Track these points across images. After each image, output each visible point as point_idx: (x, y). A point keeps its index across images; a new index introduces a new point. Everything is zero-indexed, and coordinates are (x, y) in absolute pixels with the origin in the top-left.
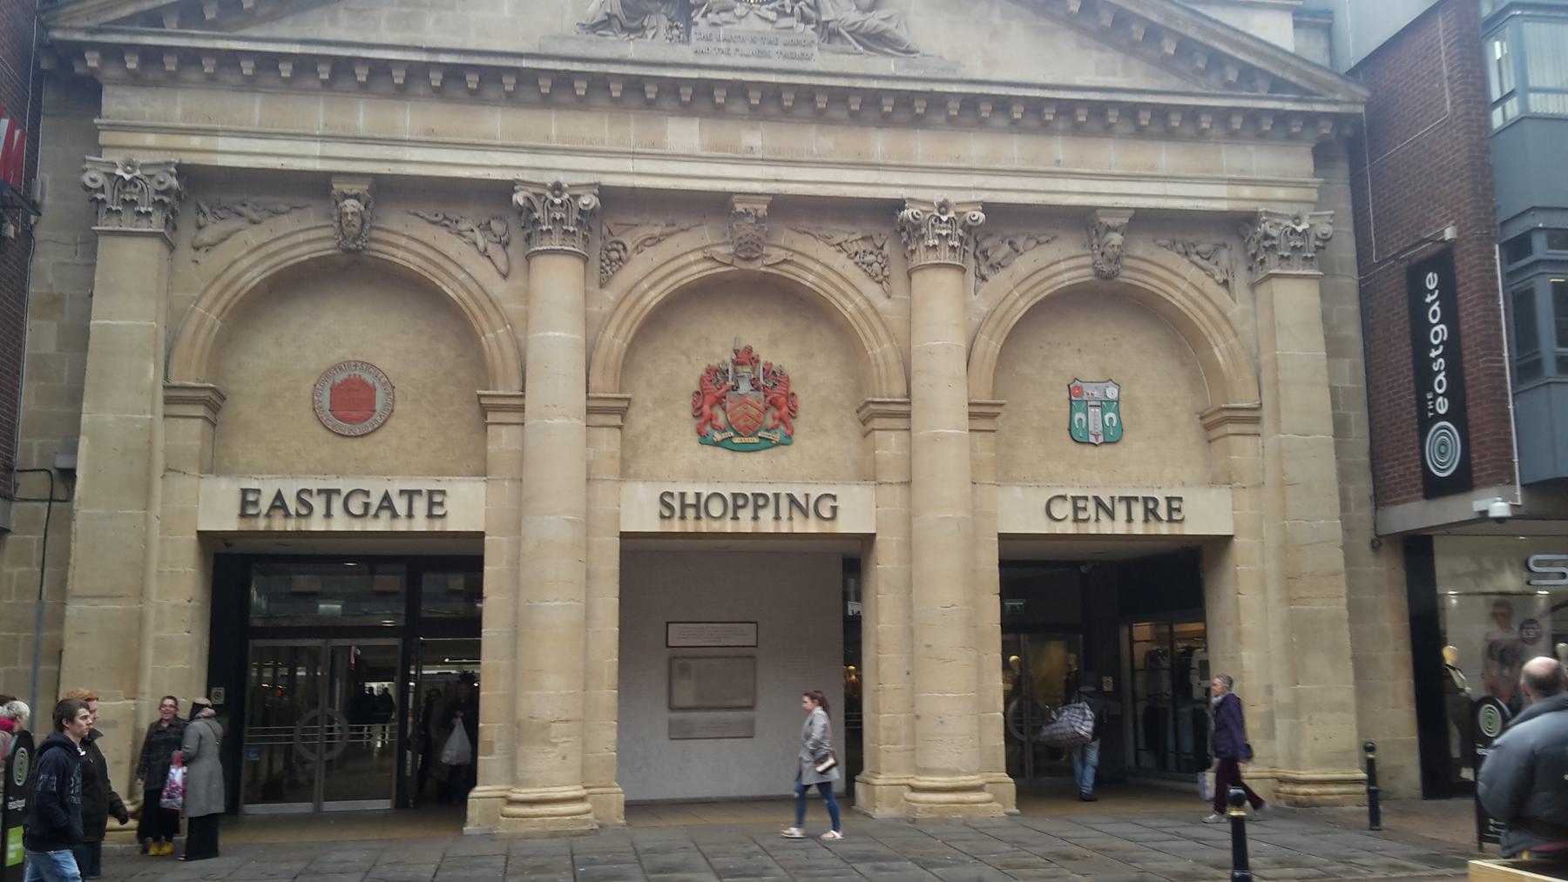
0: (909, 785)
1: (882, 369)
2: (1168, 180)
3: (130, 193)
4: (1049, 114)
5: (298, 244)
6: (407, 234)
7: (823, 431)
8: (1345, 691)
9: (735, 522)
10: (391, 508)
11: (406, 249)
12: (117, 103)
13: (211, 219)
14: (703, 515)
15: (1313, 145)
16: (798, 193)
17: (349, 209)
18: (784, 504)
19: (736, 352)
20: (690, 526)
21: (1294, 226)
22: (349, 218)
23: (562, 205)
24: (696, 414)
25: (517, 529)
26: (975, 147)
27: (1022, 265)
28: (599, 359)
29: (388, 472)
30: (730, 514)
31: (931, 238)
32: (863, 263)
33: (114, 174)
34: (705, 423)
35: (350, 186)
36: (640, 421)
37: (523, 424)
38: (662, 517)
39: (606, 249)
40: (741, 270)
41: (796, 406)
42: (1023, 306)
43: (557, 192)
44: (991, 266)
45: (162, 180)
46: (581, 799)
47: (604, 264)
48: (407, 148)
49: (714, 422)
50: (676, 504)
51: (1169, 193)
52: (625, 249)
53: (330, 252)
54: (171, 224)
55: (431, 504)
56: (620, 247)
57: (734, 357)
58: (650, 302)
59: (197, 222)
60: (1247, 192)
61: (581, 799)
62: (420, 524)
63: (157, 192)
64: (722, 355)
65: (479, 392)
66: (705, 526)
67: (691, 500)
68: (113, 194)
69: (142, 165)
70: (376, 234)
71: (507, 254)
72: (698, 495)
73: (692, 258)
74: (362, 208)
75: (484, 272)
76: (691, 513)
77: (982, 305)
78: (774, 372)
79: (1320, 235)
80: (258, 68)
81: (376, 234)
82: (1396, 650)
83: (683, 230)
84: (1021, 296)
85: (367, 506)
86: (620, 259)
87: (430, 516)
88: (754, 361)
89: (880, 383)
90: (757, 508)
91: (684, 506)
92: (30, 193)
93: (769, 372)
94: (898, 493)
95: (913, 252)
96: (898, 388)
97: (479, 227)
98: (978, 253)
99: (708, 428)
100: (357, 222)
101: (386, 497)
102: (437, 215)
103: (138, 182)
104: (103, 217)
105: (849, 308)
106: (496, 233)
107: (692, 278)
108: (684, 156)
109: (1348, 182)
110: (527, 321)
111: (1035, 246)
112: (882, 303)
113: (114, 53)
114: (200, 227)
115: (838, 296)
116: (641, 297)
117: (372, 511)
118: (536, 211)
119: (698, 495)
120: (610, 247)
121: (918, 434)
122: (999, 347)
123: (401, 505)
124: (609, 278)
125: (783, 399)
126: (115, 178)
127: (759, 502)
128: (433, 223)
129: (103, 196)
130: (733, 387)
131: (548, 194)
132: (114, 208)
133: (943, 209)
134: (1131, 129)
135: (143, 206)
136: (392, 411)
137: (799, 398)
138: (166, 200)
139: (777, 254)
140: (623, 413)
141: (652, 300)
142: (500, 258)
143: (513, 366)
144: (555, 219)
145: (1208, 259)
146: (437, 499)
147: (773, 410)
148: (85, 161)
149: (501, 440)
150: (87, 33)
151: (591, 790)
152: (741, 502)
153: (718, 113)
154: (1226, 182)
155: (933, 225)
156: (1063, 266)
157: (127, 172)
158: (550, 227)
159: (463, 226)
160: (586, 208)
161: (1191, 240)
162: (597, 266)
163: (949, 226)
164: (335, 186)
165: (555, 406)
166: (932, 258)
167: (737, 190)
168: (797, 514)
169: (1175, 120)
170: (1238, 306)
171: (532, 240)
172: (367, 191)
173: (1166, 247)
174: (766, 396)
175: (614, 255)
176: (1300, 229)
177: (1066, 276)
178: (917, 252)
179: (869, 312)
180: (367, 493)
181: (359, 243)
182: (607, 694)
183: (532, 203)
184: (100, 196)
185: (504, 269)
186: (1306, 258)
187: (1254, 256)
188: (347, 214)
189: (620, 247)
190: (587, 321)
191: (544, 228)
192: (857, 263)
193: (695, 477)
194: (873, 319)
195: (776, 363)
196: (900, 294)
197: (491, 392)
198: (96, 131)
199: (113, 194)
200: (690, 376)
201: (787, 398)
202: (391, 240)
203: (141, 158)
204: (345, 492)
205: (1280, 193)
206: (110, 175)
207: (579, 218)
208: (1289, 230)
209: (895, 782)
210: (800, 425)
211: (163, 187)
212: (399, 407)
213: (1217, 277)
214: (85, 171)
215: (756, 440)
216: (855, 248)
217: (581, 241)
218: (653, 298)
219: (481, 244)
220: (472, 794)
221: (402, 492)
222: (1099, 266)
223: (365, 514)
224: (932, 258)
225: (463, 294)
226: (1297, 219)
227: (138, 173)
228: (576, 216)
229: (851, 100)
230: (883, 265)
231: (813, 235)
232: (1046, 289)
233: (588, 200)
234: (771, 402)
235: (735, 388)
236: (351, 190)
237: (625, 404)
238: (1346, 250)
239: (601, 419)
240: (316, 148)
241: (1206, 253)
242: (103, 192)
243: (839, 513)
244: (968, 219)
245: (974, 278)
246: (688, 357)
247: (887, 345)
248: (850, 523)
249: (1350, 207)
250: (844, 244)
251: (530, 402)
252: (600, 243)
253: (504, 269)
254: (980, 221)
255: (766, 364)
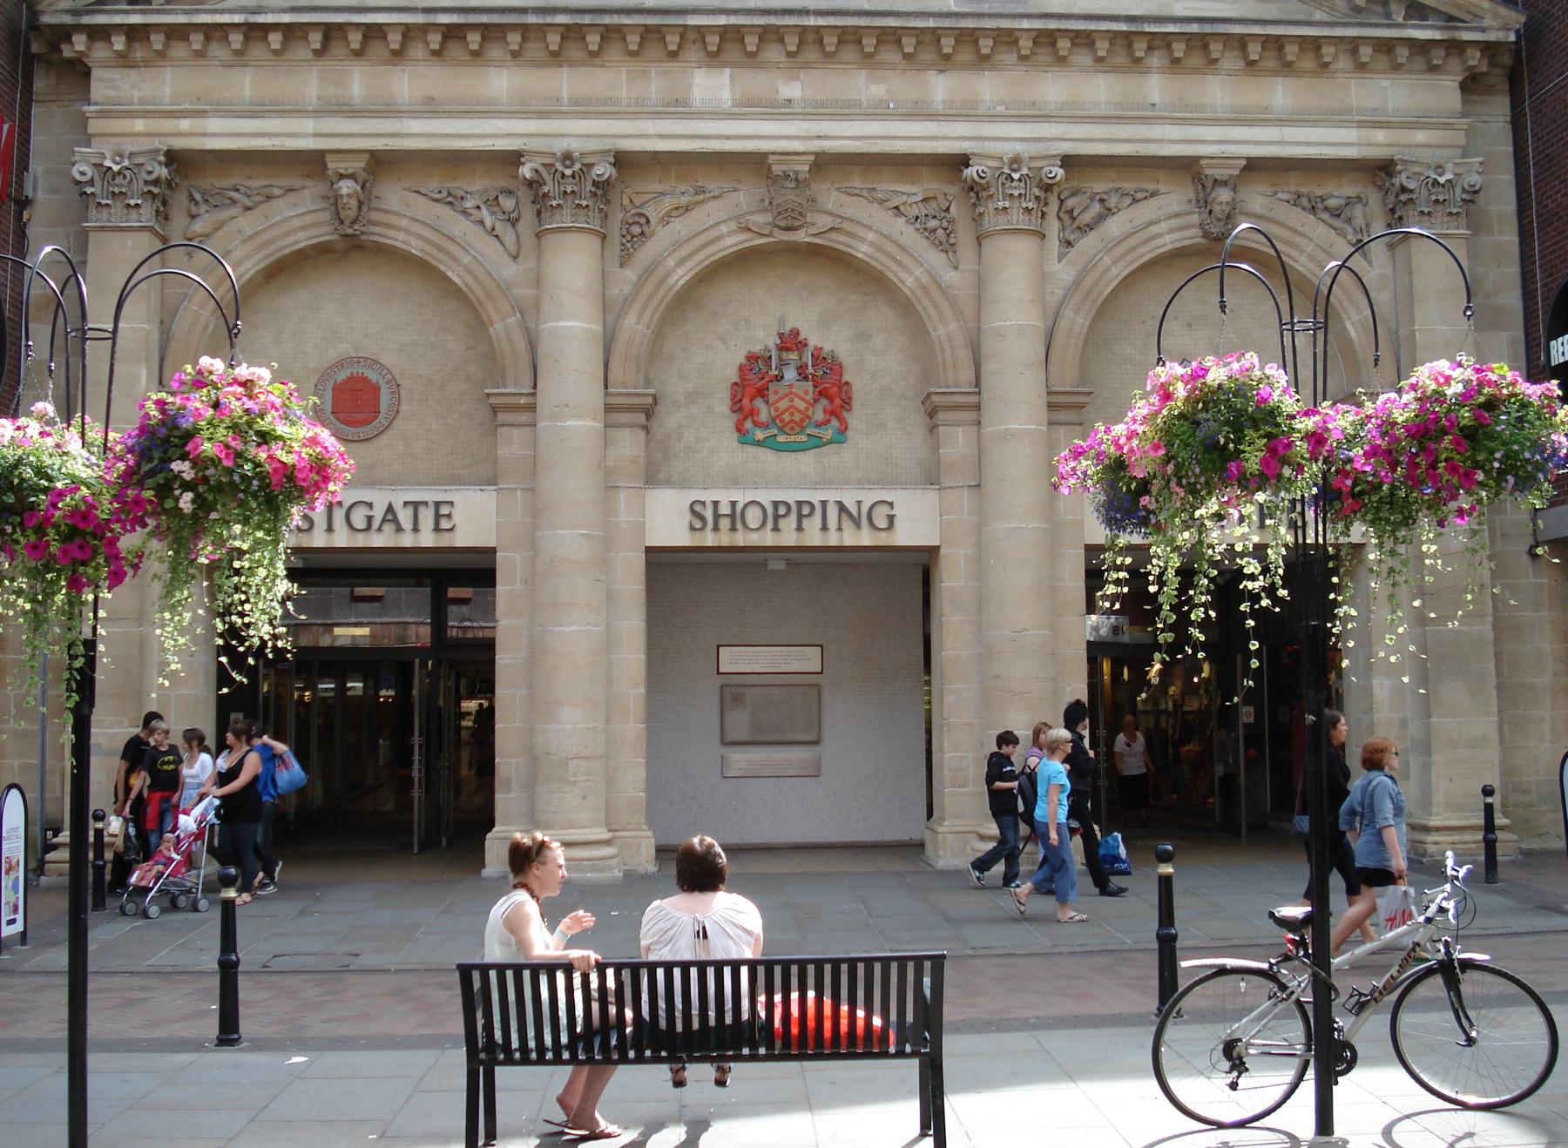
0: (977, 833)
1: (948, 352)
2: (1284, 123)
3: (120, 185)
4: (1140, 50)
5: (294, 231)
6: (408, 214)
7: (882, 426)
8: (1485, 725)
9: (776, 533)
10: (395, 520)
11: (407, 232)
12: (108, 84)
13: (204, 207)
14: (739, 525)
15: (1461, 79)
16: (846, 151)
17: (344, 191)
18: (832, 513)
19: (781, 336)
20: (725, 539)
21: (1434, 176)
22: (345, 201)
23: (573, 176)
24: (734, 409)
25: (533, 544)
26: (1053, 87)
27: (1114, 226)
28: (619, 349)
29: (394, 482)
30: (770, 525)
31: (1001, 198)
32: (925, 229)
33: (102, 165)
34: (745, 418)
35: (345, 165)
36: (669, 419)
37: (535, 425)
38: (692, 528)
39: (627, 223)
40: (782, 242)
41: (850, 398)
42: (1119, 272)
43: (568, 163)
44: (1079, 228)
45: (151, 169)
46: (608, 843)
47: (624, 241)
48: (405, 120)
49: (755, 418)
50: (709, 514)
51: (1286, 139)
52: (648, 222)
53: (328, 238)
54: (163, 215)
55: (438, 516)
56: (643, 220)
57: (778, 342)
58: (677, 282)
59: (189, 211)
60: (1380, 136)
61: (608, 843)
62: (427, 539)
63: (146, 183)
64: (764, 338)
65: (487, 391)
66: (741, 539)
67: (725, 509)
68: (103, 186)
69: (131, 154)
70: (374, 216)
71: (516, 232)
72: (734, 504)
73: (724, 229)
74: (359, 188)
75: (490, 251)
76: (725, 523)
77: (1063, 272)
78: (824, 358)
79: (1467, 188)
80: (247, 38)
81: (374, 216)
82: (1555, 675)
83: (714, 197)
84: (1114, 263)
85: (370, 519)
86: (642, 233)
87: (437, 529)
88: (801, 345)
89: (945, 370)
90: (800, 517)
91: (717, 516)
92: (22, 187)
93: (818, 357)
94: (963, 502)
95: (981, 215)
96: (967, 375)
97: (485, 202)
98: (1062, 215)
99: (748, 424)
100: (354, 203)
101: (390, 509)
102: (440, 192)
103: (127, 173)
104: (93, 213)
105: (908, 280)
106: (505, 209)
107: (726, 253)
108: (711, 113)
109: (1509, 119)
110: (538, 309)
111: (1130, 205)
112: (949, 276)
113: (100, 33)
114: (193, 217)
115: (895, 268)
116: (667, 276)
117: (376, 524)
118: (545, 184)
119: (734, 504)
120: (631, 221)
121: (988, 429)
122: (1087, 324)
123: (405, 517)
124: (630, 255)
125: (835, 390)
126: (105, 169)
127: (803, 510)
128: (437, 201)
129: (93, 190)
130: (777, 376)
131: (559, 167)
132: (103, 202)
133: (1015, 166)
134: (1241, 64)
135: (132, 198)
136: (398, 412)
137: (854, 388)
138: (156, 190)
139: (823, 222)
140: (649, 412)
141: (680, 279)
142: (509, 237)
143: (525, 361)
144: (565, 191)
145: (1339, 215)
146: (444, 510)
147: (824, 402)
148: (73, 152)
149: (512, 444)
150: (73, 15)
151: (617, 834)
152: (782, 511)
153: (752, 59)
154: (1355, 124)
155: (1003, 184)
156: (1163, 226)
157: (117, 164)
158: (561, 202)
159: (469, 204)
160: (600, 179)
161: (1319, 192)
162: (618, 239)
163: (1023, 185)
164: (330, 165)
165: (566, 406)
166: (1002, 222)
167: (773, 150)
168: (847, 524)
169: (1291, 51)
170: (1376, 267)
171: (543, 216)
172: (364, 169)
173: (1288, 202)
174: (815, 386)
175: (636, 230)
176: (1442, 180)
177: (1168, 238)
178: (986, 215)
179: (932, 287)
180: (370, 505)
181: (356, 227)
182: (632, 728)
183: (541, 175)
184: (89, 190)
185: (513, 249)
186: (1450, 214)
187: (1393, 211)
188: (342, 196)
189: (643, 220)
190: (605, 306)
191: (554, 203)
192: (918, 230)
193: (734, 482)
194: (937, 295)
195: (827, 348)
196: (968, 264)
197: (502, 391)
198: (84, 120)
199: (103, 186)
200: (726, 363)
201: (839, 387)
202: (392, 222)
203: (130, 146)
204: (346, 505)
205: (1421, 136)
206: (98, 166)
207: (593, 189)
208: (1430, 180)
209: (959, 829)
210: (855, 419)
211: (153, 177)
212: (404, 407)
213: (1350, 237)
214: (73, 164)
215: (804, 438)
216: (916, 212)
217: (597, 215)
218: (681, 276)
219: (488, 223)
220: (489, 836)
221: (406, 503)
222: (1207, 227)
223: (369, 527)
224: (1002, 222)
225: (470, 280)
226: (1440, 169)
227: (126, 163)
228: (589, 187)
229: (905, 40)
230: (948, 231)
231: (866, 198)
232: (1146, 254)
233: (603, 170)
234: (820, 392)
235: (780, 378)
236: (346, 169)
237: (650, 400)
238: (1502, 201)
239: (623, 418)
240: (308, 125)
241: (1338, 209)
242: (93, 185)
243: (897, 521)
244: (1043, 176)
245: (1058, 243)
246: (725, 342)
247: (953, 325)
248: (911, 532)
249: (1510, 149)
250: (902, 208)
251: (543, 400)
252: (620, 215)
253: (514, 254)
254: (1058, 178)
255: (816, 349)
